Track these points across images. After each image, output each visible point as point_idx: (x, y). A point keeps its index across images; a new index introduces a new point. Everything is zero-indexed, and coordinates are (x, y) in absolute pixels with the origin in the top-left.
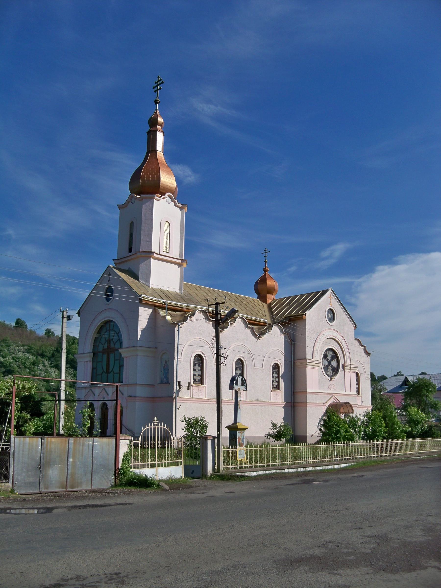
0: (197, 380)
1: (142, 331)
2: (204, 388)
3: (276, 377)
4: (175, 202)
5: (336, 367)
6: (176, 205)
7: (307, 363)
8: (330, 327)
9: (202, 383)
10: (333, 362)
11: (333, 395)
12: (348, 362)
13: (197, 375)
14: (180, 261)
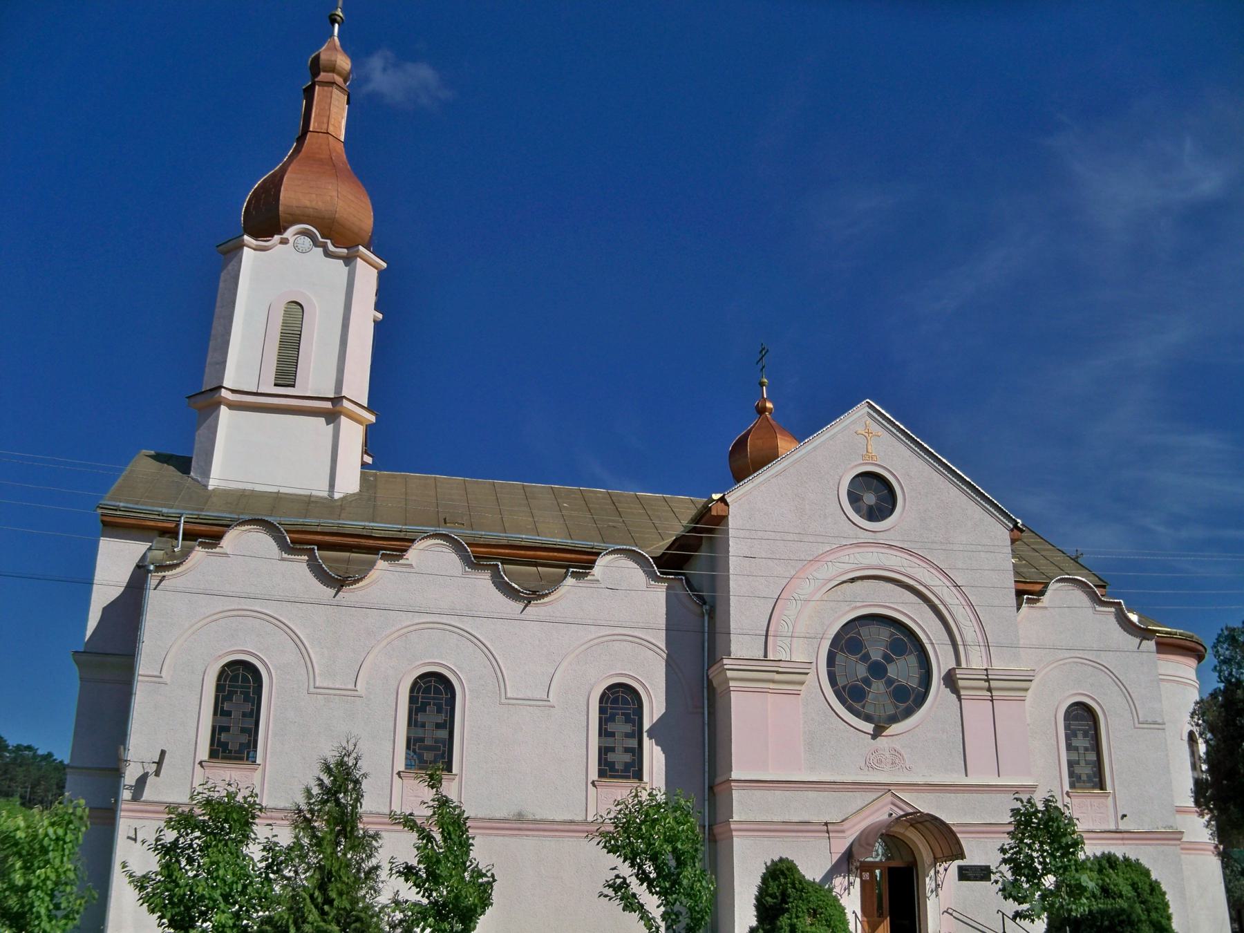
0: (1084, 778)
1: (106, 610)
2: (1110, 799)
3: (627, 735)
4: (324, 246)
5: (914, 683)
6: (328, 254)
7: (729, 674)
8: (864, 537)
9: (1102, 786)
10: (880, 668)
11: (887, 788)
12: (975, 660)
13: (1082, 763)
14: (328, 405)
